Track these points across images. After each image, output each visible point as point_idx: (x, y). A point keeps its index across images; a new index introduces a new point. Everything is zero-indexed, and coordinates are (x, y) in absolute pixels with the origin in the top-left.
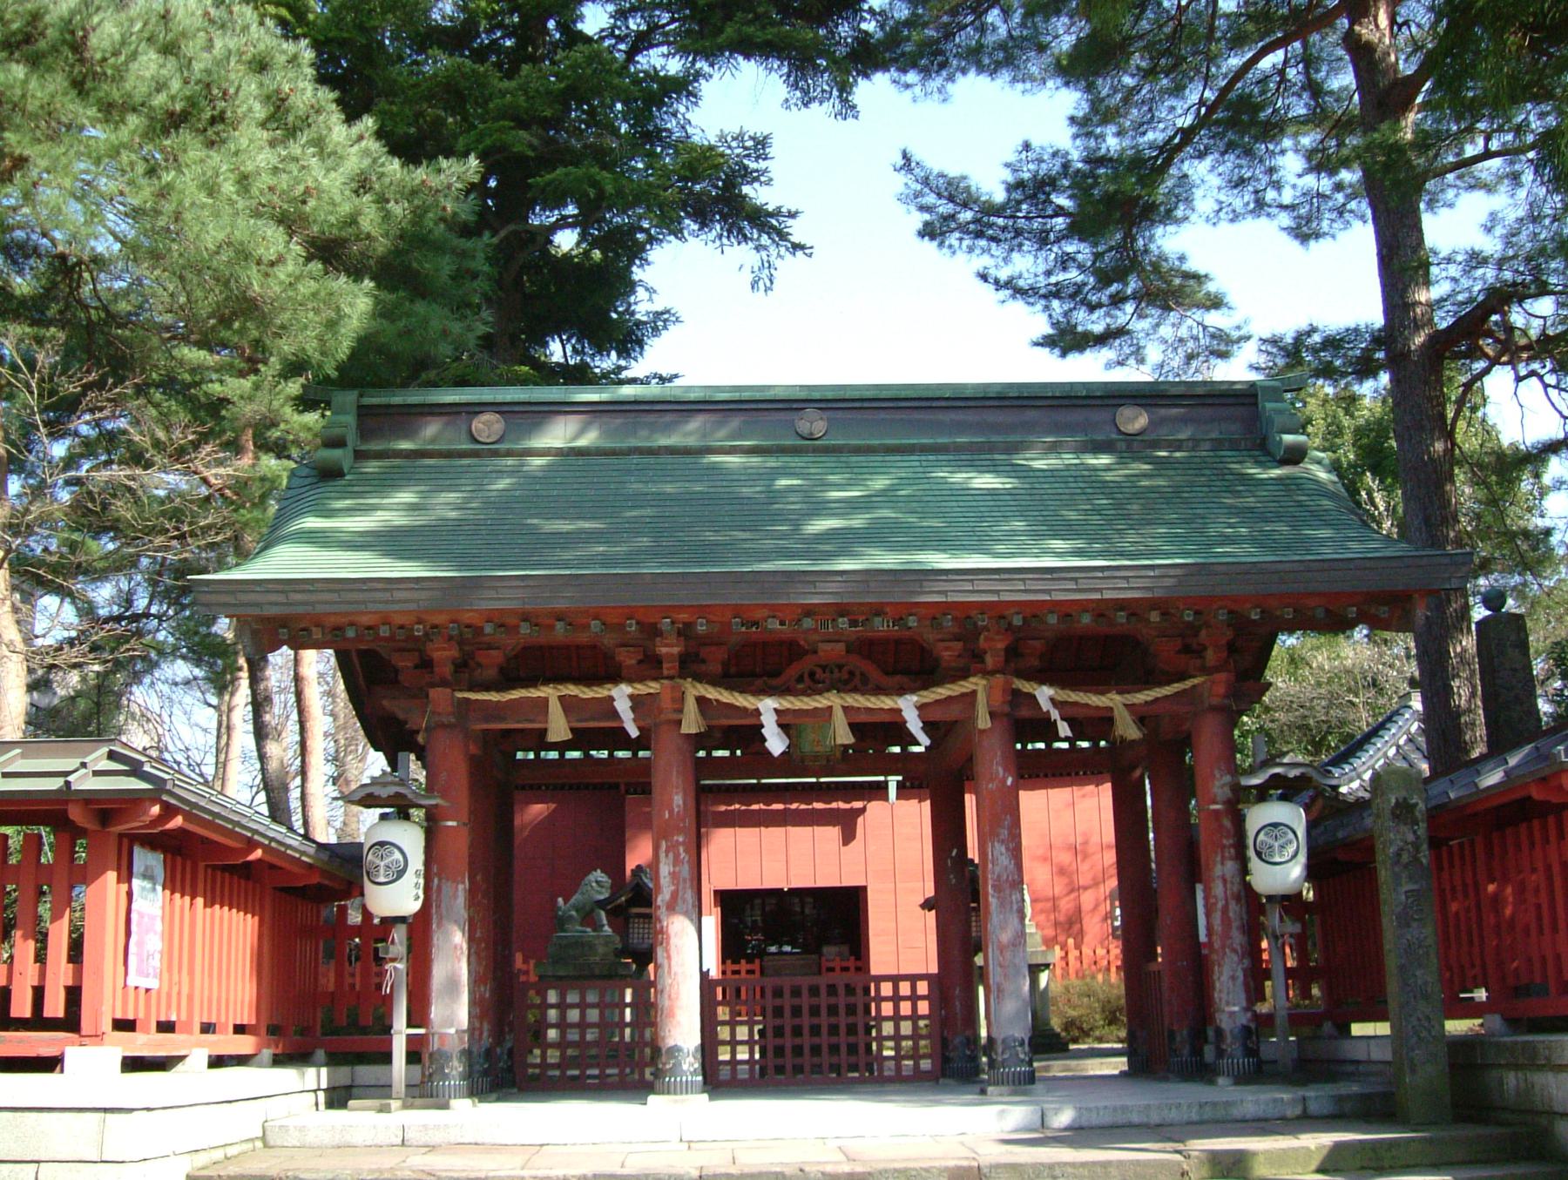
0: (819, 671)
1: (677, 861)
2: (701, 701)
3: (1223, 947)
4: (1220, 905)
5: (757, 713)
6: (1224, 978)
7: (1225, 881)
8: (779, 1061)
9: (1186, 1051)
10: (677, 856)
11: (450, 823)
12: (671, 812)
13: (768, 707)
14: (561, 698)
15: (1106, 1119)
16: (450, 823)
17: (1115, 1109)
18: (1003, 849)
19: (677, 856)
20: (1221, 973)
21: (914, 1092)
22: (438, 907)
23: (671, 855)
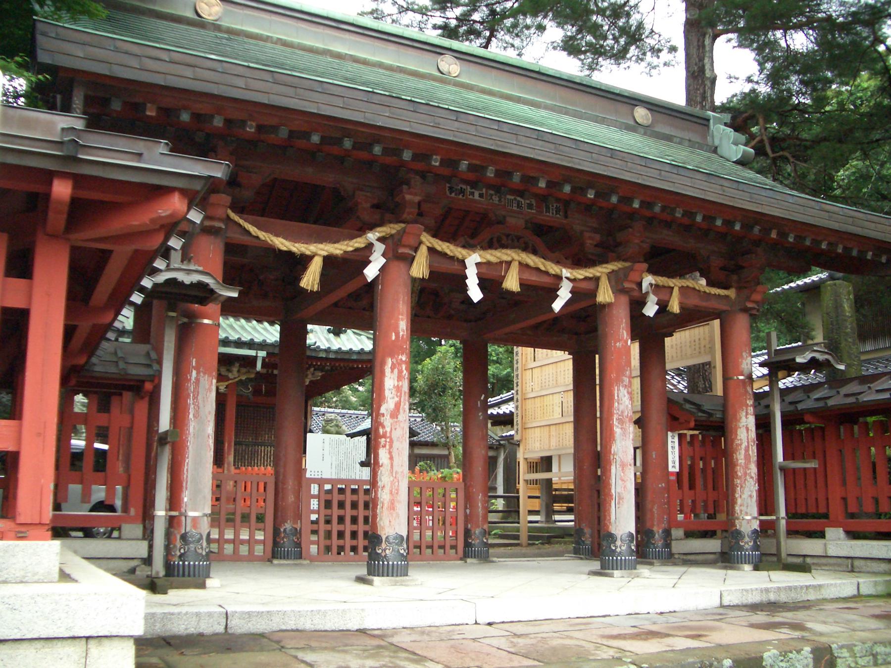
0: (504, 238)
1: (400, 378)
2: (432, 250)
3: (745, 474)
4: (743, 446)
5: (462, 263)
6: (745, 496)
7: (747, 429)
8: (354, 543)
9: (660, 544)
10: (400, 372)
11: (206, 321)
12: (397, 334)
13: (473, 260)
14: (681, 288)
15: (755, 598)
16: (206, 321)
17: (762, 591)
18: (625, 392)
19: (400, 372)
20: (742, 492)
21: (431, 567)
22: (195, 398)
23: (396, 371)
